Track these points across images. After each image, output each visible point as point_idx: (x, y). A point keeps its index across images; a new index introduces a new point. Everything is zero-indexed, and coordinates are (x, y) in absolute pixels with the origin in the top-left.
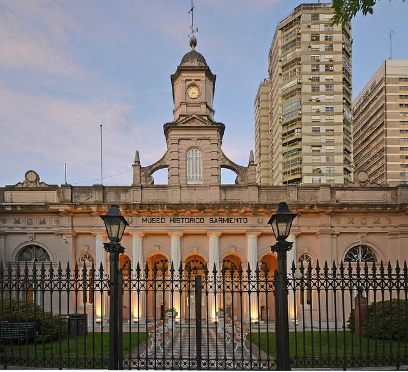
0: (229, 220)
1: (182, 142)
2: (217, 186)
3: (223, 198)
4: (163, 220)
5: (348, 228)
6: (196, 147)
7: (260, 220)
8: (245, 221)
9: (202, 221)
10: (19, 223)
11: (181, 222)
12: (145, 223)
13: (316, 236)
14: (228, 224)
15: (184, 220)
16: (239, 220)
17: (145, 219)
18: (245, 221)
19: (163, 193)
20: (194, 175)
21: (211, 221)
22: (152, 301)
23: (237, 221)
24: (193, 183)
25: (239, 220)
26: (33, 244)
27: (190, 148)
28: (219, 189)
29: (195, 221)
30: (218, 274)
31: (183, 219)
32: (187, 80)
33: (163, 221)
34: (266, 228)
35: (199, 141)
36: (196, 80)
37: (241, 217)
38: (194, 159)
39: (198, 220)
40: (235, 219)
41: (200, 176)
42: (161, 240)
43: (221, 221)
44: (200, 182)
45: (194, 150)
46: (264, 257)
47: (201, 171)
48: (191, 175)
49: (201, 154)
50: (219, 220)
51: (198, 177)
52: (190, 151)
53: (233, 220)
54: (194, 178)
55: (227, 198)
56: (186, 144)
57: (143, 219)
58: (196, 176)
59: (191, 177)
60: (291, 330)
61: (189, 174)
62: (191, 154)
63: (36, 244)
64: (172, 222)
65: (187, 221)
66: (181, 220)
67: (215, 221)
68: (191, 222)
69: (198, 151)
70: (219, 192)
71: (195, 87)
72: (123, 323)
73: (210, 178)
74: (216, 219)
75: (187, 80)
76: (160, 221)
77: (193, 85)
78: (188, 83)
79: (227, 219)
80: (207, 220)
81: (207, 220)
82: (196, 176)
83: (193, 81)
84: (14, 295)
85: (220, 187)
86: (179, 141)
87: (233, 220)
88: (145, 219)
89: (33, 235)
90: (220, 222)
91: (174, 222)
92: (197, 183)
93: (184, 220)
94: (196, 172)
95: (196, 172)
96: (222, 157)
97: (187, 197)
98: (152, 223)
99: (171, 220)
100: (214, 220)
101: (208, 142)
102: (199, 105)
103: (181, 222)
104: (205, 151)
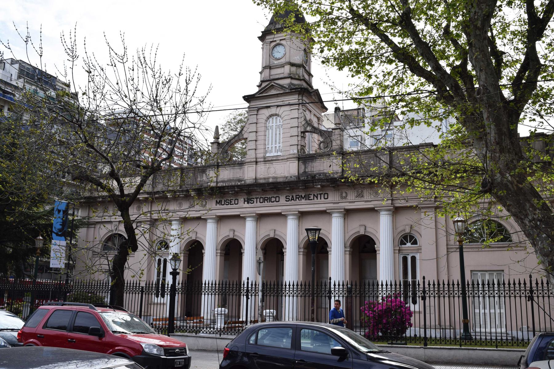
0: (307, 197)
1: (262, 111)
2: (294, 158)
3: (302, 171)
5: (356, 203)
6: (276, 115)
8: (326, 197)
10: (363, 196)
11: (255, 202)
12: (218, 206)
16: (319, 196)
18: (326, 197)
19: (239, 170)
20: (274, 146)
23: (317, 197)
24: (272, 155)
25: (319, 196)
26: (116, 232)
27: (271, 116)
30: (470, 286)
32: (271, 42)
33: (236, 203)
36: (281, 40)
37: (321, 192)
38: (274, 127)
39: (273, 199)
40: (314, 195)
42: (234, 225)
43: (298, 198)
44: (279, 154)
45: (275, 117)
47: (281, 141)
48: (270, 146)
49: (281, 121)
50: (296, 198)
51: (278, 148)
52: (271, 119)
54: (274, 148)
55: (307, 170)
56: (266, 113)
57: (217, 201)
58: (276, 147)
59: (270, 149)
61: (268, 144)
62: (271, 122)
63: (119, 233)
64: (246, 203)
65: (261, 201)
66: (255, 200)
69: (279, 118)
71: (281, 46)
73: (288, 148)
75: (271, 42)
76: (233, 203)
77: (279, 44)
82: (276, 147)
83: (278, 42)
86: (258, 111)
87: (312, 197)
89: (117, 223)
91: (248, 203)
92: (276, 154)
94: (276, 141)
95: (276, 141)
98: (225, 206)
99: (245, 201)
101: (287, 108)
102: (282, 66)
103: (255, 202)
104: (285, 118)
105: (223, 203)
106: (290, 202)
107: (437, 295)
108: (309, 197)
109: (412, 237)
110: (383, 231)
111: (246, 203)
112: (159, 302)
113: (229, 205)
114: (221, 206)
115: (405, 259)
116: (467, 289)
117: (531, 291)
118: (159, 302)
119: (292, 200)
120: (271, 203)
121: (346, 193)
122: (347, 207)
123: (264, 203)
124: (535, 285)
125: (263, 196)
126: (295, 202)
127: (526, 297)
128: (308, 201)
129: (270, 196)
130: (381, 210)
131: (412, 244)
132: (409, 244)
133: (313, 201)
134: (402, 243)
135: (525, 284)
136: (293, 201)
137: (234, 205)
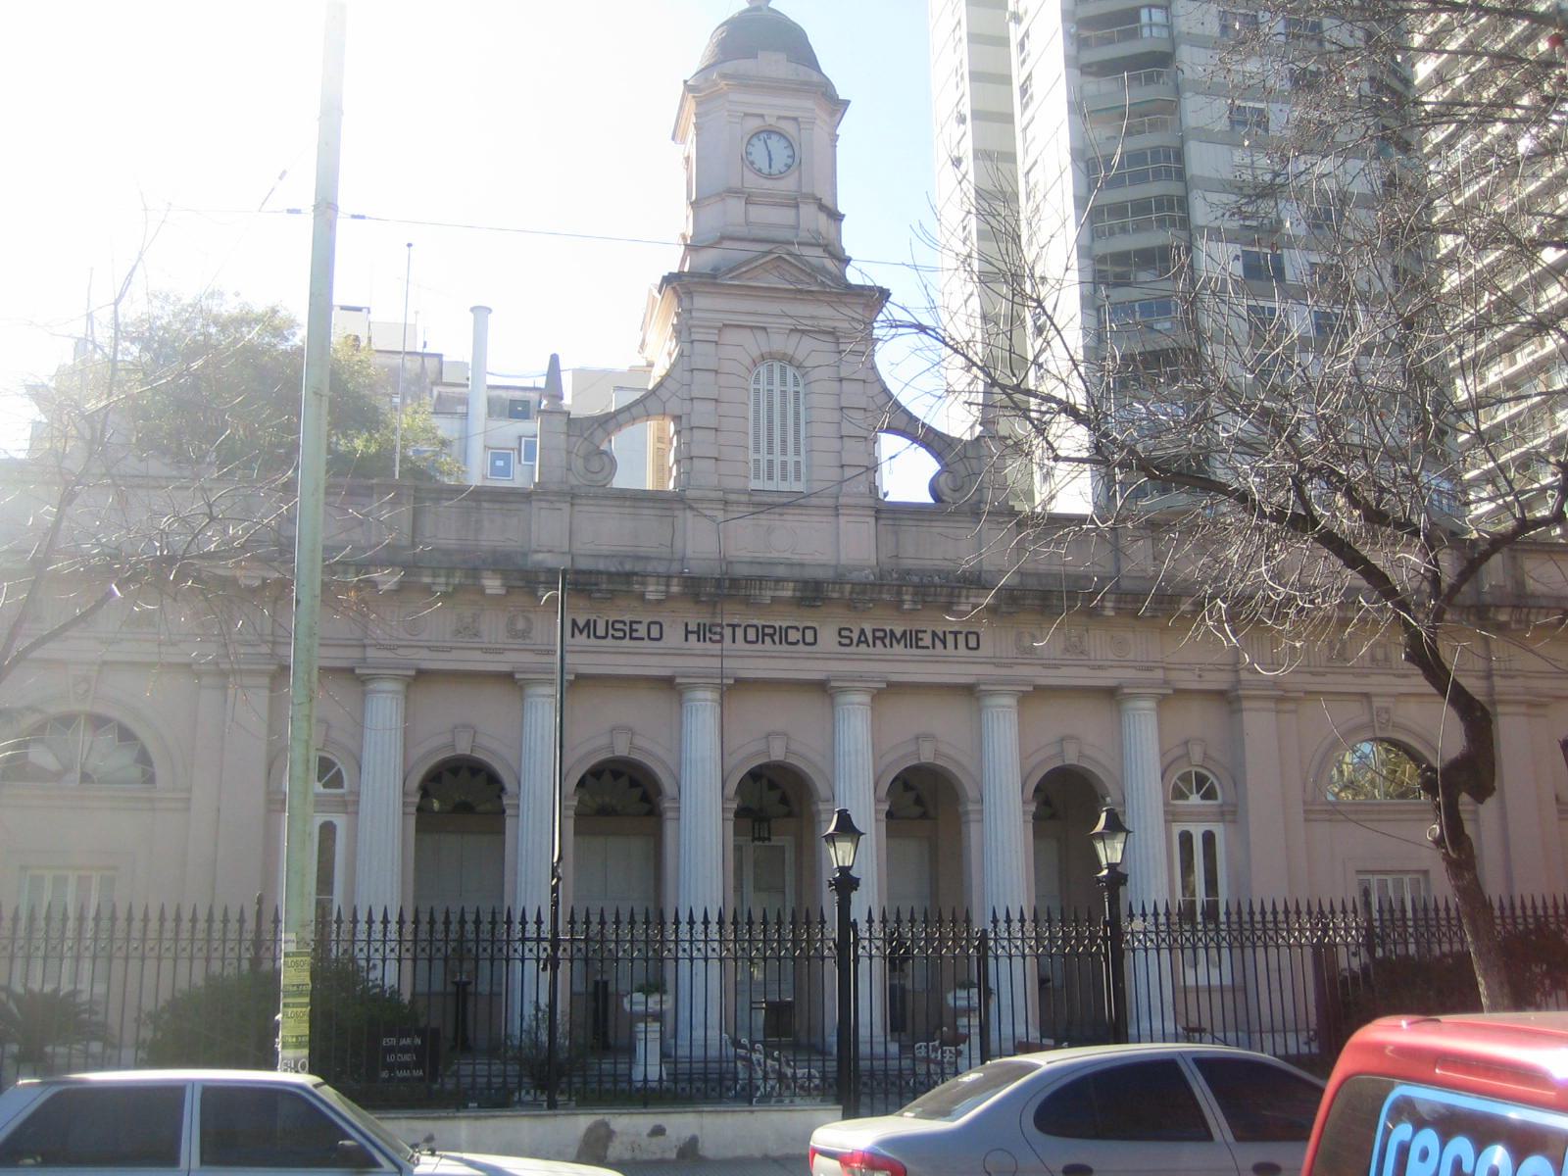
4: (715, 629)
5: (454, 654)
7: (521, 625)
8: (973, 643)
9: (809, 637)
13: (1230, 703)
14: (909, 651)
15: (739, 632)
17: (581, 625)
18: (973, 643)
21: (844, 637)
22: (878, 972)
25: (950, 639)
28: (872, 521)
29: (781, 635)
30: (452, 927)
31: (734, 626)
33: (655, 633)
34: (1318, 679)
35: (795, 337)
36: (779, 118)
40: (934, 634)
41: (757, 461)
43: (882, 639)
46: (755, 775)
50: (875, 638)
53: (927, 640)
60: (864, 1064)
64: (693, 638)
65: (752, 636)
66: (728, 632)
67: (859, 642)
68: (767, 639)
69: (790, 371)
70: (873, 532)
72: (835, 1069)
74: (862, 632)
76: (642, 631)
78: (754, 124)
79: (588, 623)
80: (828, 637)
81: (828, 637)
83: (771, 121)
84: (1436, 948)
85: (878, 511)
87: (927, 640)
88: (581, 625)
90: (878, 642)
92: (784, 487)
93: (739, 632)
94: (784, 441)
95: (784, 441)
96: (881, 399)
97: (748, 543)
98: (609, 641)
99: (687, 632)
100: (855, 636)
105: (601, 631)
106: (853, 649)
107: (408, 955)
108: (918, 639)
109: (1201, 780)
110: (1139, 756)
111: (693, 638)
112: (1203, 982)
113: (627, 642)
114: (593, 641)
115: (1186, 839)
116: (334, 937)
117: (555, 943)
118: (1203, 982)
119: (859, 642)
120: (785, 647)
121: (528, 620)
122: (895, 678)
123: (759, 646)
124: (442, 927)
125: (759, 622)
126: (871, 650)
127: (538, 960)
128: (914, 651)
129: (784, 625)
130: (693, 687)
131: (1203, 797)
132: (1195, 799)
133: (930, 651)
134: (1179, 794)
135: (241, 920)
136: (863, 646)
137: (647, 643)
